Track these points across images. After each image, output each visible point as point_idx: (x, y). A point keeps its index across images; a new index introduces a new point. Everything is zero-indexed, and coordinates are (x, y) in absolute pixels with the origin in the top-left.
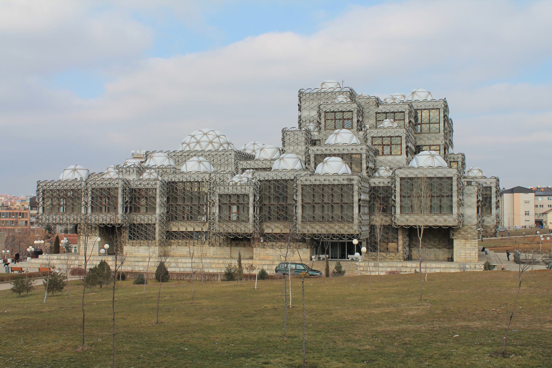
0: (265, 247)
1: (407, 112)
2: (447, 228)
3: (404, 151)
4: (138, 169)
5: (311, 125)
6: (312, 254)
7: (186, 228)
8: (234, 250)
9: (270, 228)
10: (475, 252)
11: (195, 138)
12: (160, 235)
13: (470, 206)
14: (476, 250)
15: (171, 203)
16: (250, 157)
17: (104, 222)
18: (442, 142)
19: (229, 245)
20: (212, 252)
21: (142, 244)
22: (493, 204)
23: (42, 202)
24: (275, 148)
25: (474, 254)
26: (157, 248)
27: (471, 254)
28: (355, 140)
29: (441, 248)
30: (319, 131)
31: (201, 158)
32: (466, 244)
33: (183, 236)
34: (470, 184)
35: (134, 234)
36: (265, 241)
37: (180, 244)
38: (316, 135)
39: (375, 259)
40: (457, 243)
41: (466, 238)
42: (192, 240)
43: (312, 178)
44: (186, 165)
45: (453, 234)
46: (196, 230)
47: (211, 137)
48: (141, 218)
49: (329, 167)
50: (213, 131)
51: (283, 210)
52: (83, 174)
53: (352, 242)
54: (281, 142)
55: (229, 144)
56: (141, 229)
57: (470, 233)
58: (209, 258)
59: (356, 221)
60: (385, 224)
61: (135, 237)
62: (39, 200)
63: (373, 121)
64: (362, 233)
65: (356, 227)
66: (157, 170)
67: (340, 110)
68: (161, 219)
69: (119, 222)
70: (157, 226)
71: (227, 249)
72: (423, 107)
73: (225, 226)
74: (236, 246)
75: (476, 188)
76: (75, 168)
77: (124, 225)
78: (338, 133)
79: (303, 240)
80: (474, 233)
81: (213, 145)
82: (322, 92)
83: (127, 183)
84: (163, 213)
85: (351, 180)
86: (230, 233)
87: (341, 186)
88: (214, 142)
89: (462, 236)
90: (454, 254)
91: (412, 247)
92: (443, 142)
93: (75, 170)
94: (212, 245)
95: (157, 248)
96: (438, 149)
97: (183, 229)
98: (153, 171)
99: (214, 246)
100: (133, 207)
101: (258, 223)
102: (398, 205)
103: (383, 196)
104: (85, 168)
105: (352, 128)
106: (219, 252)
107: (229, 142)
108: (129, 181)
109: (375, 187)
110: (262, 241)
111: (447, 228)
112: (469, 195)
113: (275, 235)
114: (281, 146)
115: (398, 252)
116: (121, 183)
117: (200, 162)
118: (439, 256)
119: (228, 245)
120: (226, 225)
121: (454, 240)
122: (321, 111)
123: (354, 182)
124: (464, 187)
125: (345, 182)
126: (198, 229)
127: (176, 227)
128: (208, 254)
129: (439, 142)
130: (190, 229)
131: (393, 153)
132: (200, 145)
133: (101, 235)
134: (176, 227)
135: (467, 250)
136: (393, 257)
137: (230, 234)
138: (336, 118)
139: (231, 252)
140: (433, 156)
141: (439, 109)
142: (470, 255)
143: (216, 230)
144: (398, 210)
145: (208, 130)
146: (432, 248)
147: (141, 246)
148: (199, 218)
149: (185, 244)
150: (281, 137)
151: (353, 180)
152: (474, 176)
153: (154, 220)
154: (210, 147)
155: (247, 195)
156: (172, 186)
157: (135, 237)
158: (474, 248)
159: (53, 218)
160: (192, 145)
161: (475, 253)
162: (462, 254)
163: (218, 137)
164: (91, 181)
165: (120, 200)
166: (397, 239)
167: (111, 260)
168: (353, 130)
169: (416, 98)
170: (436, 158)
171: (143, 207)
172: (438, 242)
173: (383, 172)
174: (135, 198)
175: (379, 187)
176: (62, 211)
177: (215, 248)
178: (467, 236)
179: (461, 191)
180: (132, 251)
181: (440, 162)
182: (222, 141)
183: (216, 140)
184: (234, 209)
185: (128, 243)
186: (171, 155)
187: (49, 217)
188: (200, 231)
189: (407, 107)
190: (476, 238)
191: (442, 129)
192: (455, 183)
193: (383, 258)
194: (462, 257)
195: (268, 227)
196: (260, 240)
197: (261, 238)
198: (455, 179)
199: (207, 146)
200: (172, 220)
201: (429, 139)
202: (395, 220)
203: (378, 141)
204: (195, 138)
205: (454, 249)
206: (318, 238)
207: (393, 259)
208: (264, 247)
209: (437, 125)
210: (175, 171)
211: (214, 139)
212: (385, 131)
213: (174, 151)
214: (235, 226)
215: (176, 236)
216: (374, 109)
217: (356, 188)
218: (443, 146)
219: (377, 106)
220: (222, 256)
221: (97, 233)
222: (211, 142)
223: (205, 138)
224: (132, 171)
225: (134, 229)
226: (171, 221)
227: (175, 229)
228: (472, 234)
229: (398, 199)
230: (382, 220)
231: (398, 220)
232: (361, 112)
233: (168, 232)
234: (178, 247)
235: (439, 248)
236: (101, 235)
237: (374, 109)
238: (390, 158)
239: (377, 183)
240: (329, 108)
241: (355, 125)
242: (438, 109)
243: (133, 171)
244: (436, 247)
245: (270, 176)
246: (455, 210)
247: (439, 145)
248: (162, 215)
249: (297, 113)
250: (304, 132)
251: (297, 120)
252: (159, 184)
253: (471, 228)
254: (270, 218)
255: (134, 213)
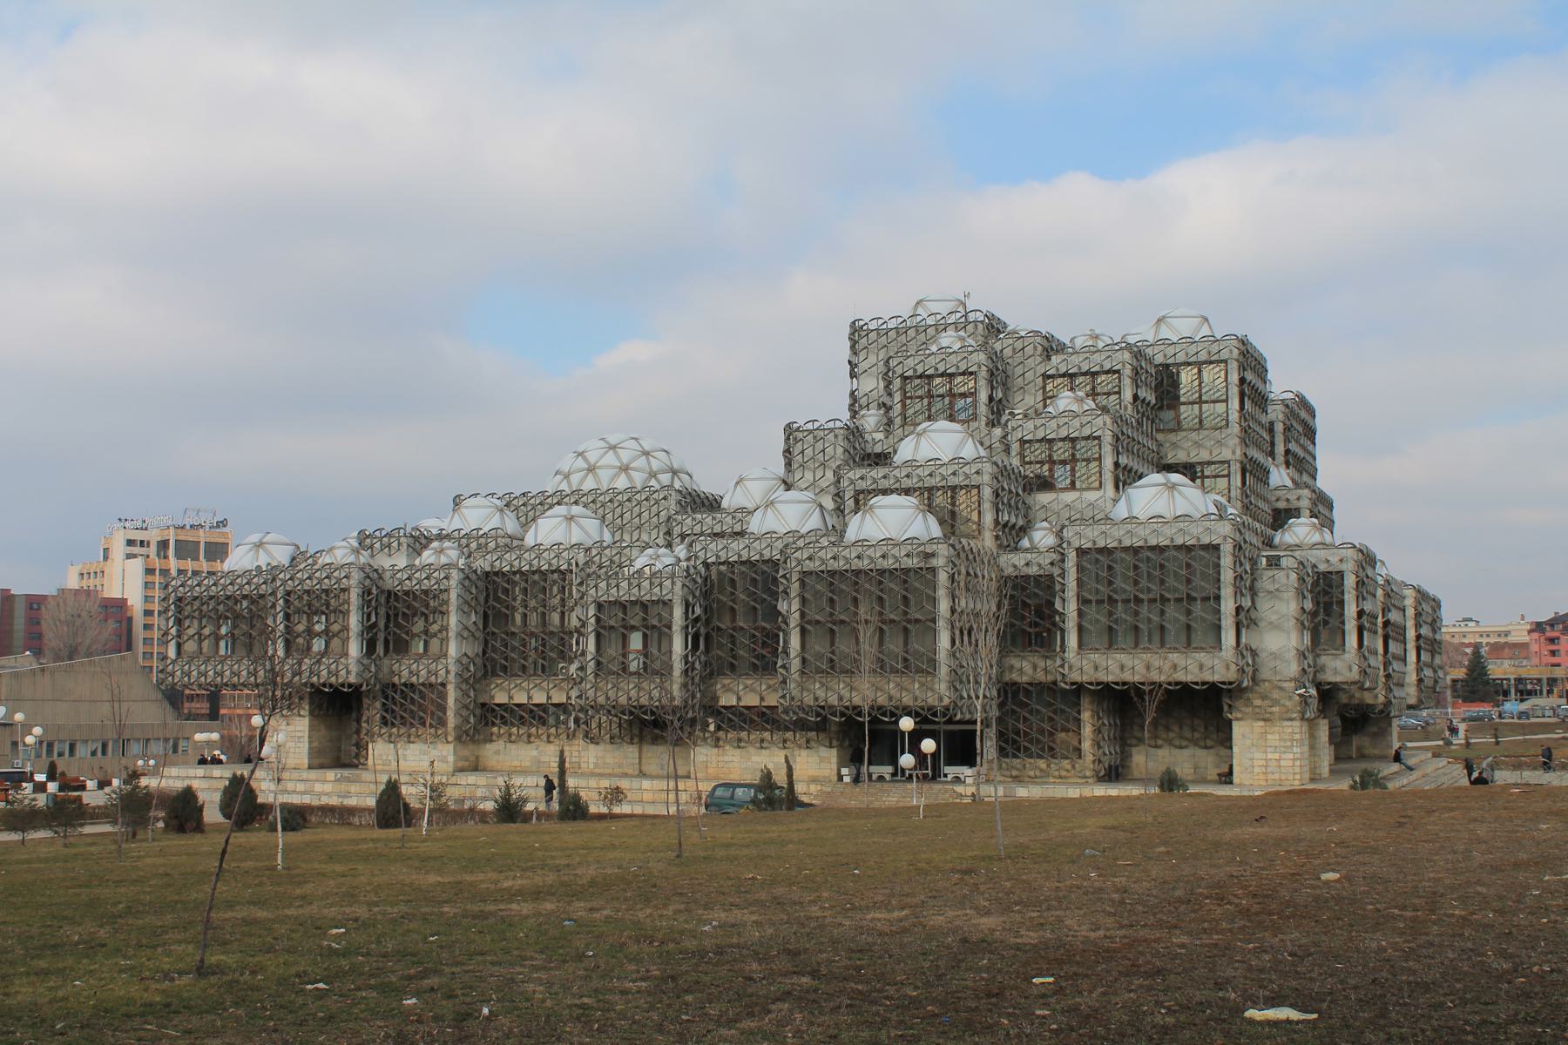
0: (721, 743)
1: (1127, 371)
2: (1099, 687)
3: (1108, 478)
4: (411, 540)
5: (871, 415)
6: (840, 765)
7: (761, 695)
8: (649, 755)
9: (734, 692)
10: (1291, 756)
11: (585, 459)
12: (457, 713)
13: (1275, 626)
14: (1295, 750)
15: (491, 628)
16: (711, 504)
17: (333, 680)
18: (1234, 453)
19: (636, 740)
20: (592, 760)
21: (412, 739)
22: (1349, 620)
23: (174, 629)
24: (773, 479)
25: (1290, 763)
26: (451, 747)
27: (1283, 763)
28: (969, 450)
29: (1211, 747)
30: (888, 433)
31: (576, 510)
32: (1266, 732)
33: (522, 717)
34: (1276, 565)
35: (393, 711)
36: (719, 728)
37: (513, 737)
38: (876, 438)
39: (1016, 777)
40: (1242, 732)
41: (1267, 716)
42: (545, 728)
43: (1018, 559)
44: (537, 526)
45: (1230, 706)
46: (555, 700)
47: (625, 456)
48: (406, 670)
49: (879, 523)
50: (636, 439)
51: (764, 644)
52: (282, 556)
53: (909, 733)
54: (782, 462)
55: (675, 472)
56: (412, 698)
57: (1276, 702)
58: (583, 775)
59: (943, 671)
60: (1043, 679)
61: (395, 718)
62: (275, 621)
63: (1031, 399)
64: (960, 704)
65: (942, 688)
66: (464, 541)
67: (1085, 369)
68: (463, 671)
69: (352, 679)
70: (451, 689)
71: (631, 751)
72: (1203, 356)
73: (817, 685)
74: (653, 744)
75: (1294, 576)
76: (260, 541)
77: (364, 688)
78: (925, 431)
79: (821, 726)
80: (1288, 703)
81: (630, 478)
82: (871, 327)
83: (372, 576)
84: (465, 654)
85: (928, 556)
86: (834, 706)
87: (904, 575)
88: (634, 469)
89: (1257, 710)
90: (1235, 762)
91: (1131, 746)
92: (1238, 452)
93: (260, 545)
94: (592, 739)
95: (451, 747)
96: (1226, 472)
97: (521, 698)
98: (447, 544)
99: (597, 743)
100: (390, 638)
101: (697, 680)
102: (1071, 624)
103: (1037, 601)
104: (288, 541)
105: (975, 417)
106: (609, 760)
107: (676, 466)
108: (380, 572)
109: (1331, 573)
110: (712, 728)
111: (1099, 687)
112: (1274, 594)
113: (745, 711)
114: (780, 470)
115: (1080, 757)
116: (356, 576)
117: (570, 519)
118: (1206, 768)
119: (831, 743)
120: (820, 682)
121: (1234, 723)
122: (890, 374)
123: (937, 562)
124: (1259, 572)
125: (912, 563)
126: (559, 697)
127: (507, 692)
128: (582, 765)
129: (1226, 454)
130: (539, 698)
131: (1078, 484)
132: (595, 475)
133: (316, 713)
134: (507, 692)
135: (1269, 750)
136: (1067, 771)
137: (644, 709)
138: (1099, 390)
139: (640, 758)
140: (1172, 487)
141: (1225, 361)
142: (1279, 766)
143: (792, 699)
144: (1072, 640)
145: (622, 436)
146: (1186, 747)
147: (410, 742)
148: (562, 668)
149: (525, 738)
150: (781, 446)
151: (933, 555)
152: (1298, 542)
153: (442, 672)
154: (622, 483)
155: (667, 604)
156: (494, 582)
157: (395, 718)
158: (1289, 744)
159: (328, 668)
160: (575, 478)
161: (1294, 760)
162: (1256, 763)
163: (646, 454)
164: (318, 570)
165: (354, 621)
166: (1078, 721)
167: (333, 779)
168: (974, 425)
169: (1165, 333)
170: (1180, 493)
171: (613, 636)
172: (1202, 730)
173: (1042, 537)
174: (396, 615)
175: (1027, 577)
176: (222, 652)
177: (601, 748)
178: (1270, 710)
179: (1248, 585)
180: (388, 756)
181: (1191, 503)
182: (655, 465)
183: (641, 462)
184: (636, 641)
185: (380, 735)
186: (509, 504)
187: (190, 668)
188: (563, 704)
189: (1127, 356)
190: (1295, 715)
191: (1234, 416)
192: (1226, 561)
193: (1038, 773)
194: (1257, 770)
195: (728, 690)
196: (708, 726)
197: (710, 720)
198: (1227, 549)
199: (614, 478)
200: (494, 674)
201: (1197, 444)
202: (1062, 666)
203: (1039, 452)
204: (585, 459)
205: (1235, 749)
206: (891, 717)
207: (1065, 777)
208: (717, 743)
209: (1221, 408)
210: (512, 543)
211: (635, 459)
212: (1076, 422)
213: (524, 494)
214: (898, 685)
215: (503, 717)
216: (1039, 367)
217: (943, 577)
218: (1238, 465)
219: (1044, 357)
220: (617, 771)
221: (304, 709)
222: (625, 469)
223: (610, 459)
224: (395, 544)
225: (393, 698)
226: (492, 676)
227: (501, 698)
228: (1284, 705)
229: (1071, 608)
230: (1035, 667)
231: (1070, 668)
232: (999, 375)
233: (483, 705)
234: (508, 745)
235: (1206, 747)
236: (316, 713)
237: (1039, 367)
238: (1069, 497)
239: (1334, 559)
240: (910, 365)
241: (983, 409)
242: (1222, 361)
243: (399, 544)
244: (1195, 743)
245: (735, 550)
246: (1229, 638)
247: (1228, 462)
248: (465, 660)
249: (846, 385)
250: (842, 431)
251: (847, 401)
252: (456, 578)
253: (1281, 689)
254: (733, 667)
255: (395, 656)
